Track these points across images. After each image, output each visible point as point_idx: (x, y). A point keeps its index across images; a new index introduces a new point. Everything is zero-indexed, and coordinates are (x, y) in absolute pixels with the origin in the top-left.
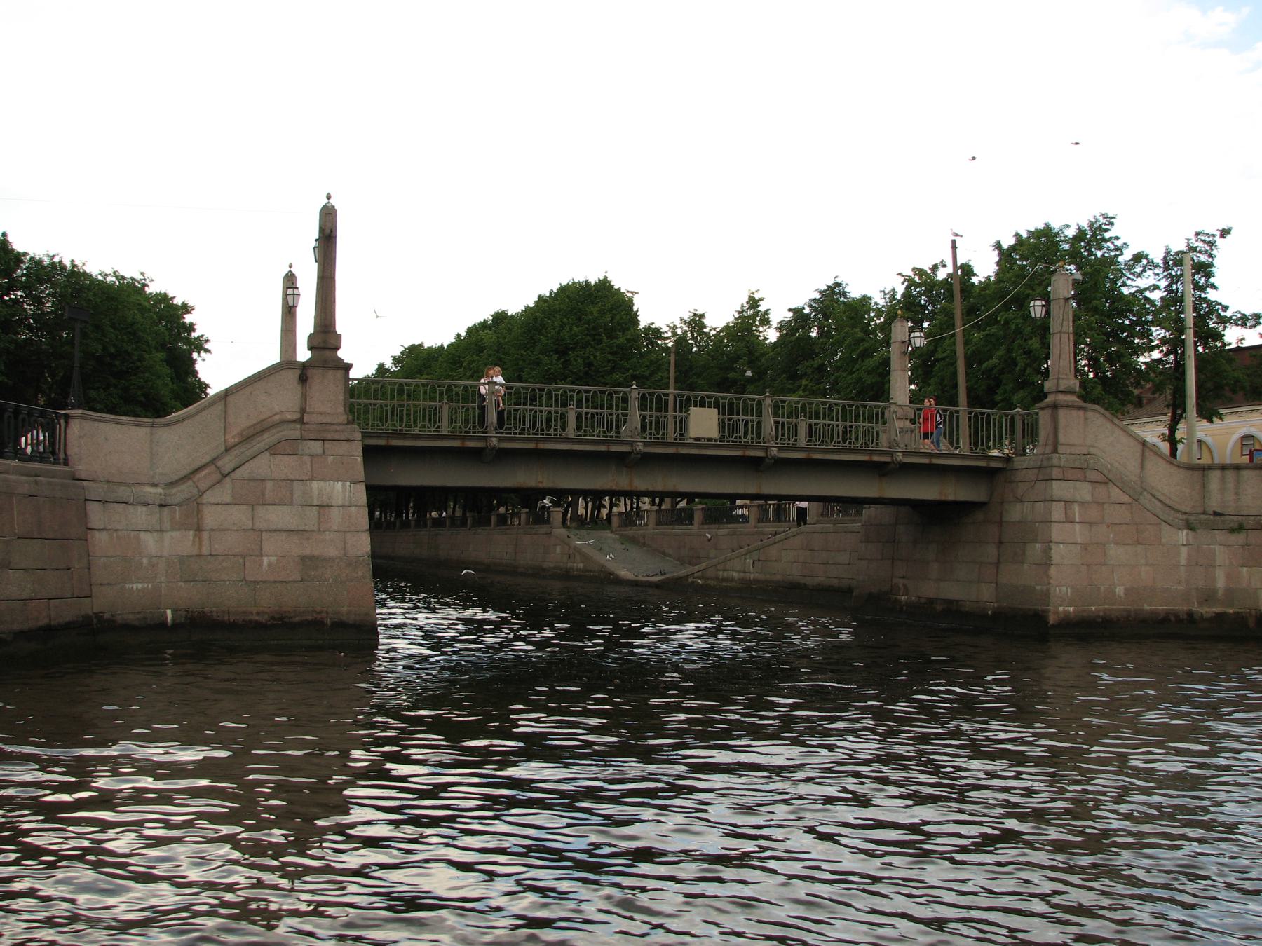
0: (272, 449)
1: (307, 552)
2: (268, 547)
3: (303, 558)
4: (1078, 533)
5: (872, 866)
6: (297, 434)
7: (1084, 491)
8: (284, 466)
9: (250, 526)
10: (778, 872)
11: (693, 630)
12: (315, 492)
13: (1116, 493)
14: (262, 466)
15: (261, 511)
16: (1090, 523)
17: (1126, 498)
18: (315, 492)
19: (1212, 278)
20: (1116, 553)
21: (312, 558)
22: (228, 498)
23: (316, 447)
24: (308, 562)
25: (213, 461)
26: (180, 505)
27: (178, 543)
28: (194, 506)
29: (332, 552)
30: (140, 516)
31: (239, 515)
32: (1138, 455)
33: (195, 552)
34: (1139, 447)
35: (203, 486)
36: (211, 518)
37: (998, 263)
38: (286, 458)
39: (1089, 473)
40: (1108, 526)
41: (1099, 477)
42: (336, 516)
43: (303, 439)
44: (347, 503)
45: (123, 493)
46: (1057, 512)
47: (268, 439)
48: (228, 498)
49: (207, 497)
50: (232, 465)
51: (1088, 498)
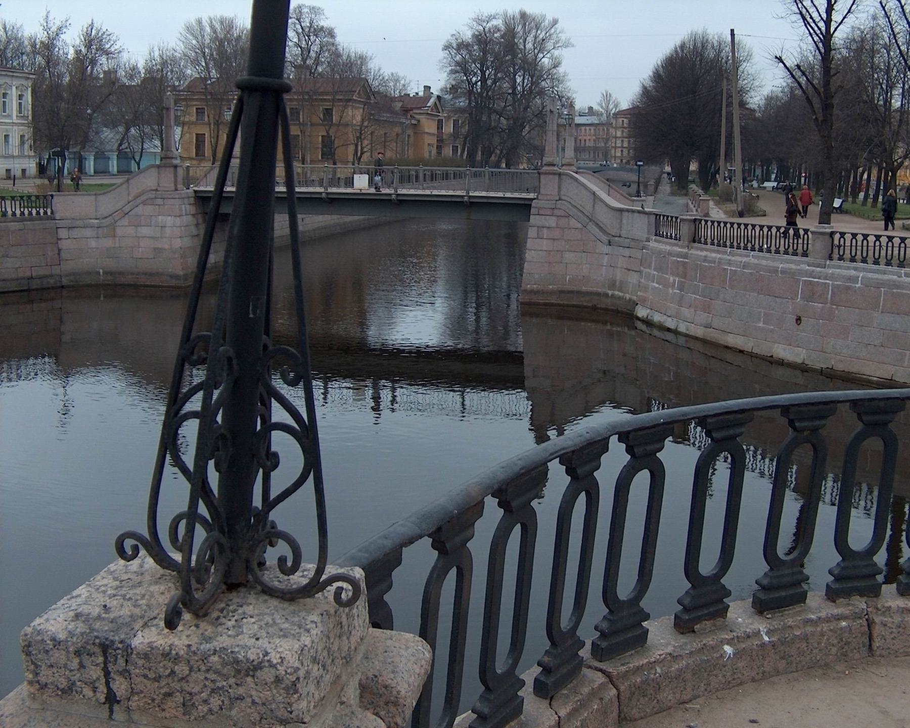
0: (144, 203)
2: (142, 244)
3: (155, 249)
4: (545, 245)
5: (425, 392)
6: (153, 196)
7: (552, 222)
8: (148, 209)
9: (135, 235)
10: (273, 474)
11: (728, 90)
12: (160, 220)
13: (573, 223)
14: (140, 210)
15: (139, 228)
16: (554, 239)
17: (579, 226)
18: (160, 220)
19: (139, 66)
20: (569, 256)
21: (157, 248)
22: (127, 224)
23: (160, 201)
24: (158, 251)
25: (121, 209)
26: (106, 227)
27: (108, 243)
28: (113, 227)
29: (166, 246)
30: (88, 232)
31: (131, 231)
32: (592, 201)
33: (113, 246)
34: (592, 196)
35: (116, 218)
36: (119, 232)
37: (645, 91)
38: (150, 206)
39: (555, 211)
41: (563, 213)
42: (168, 231)
43: (156, 198)
45: (80, 223)
46: (532, 232)
47: (143, 198)
48: (127, 224)
49: (118, 223)
50: (129, 210)
51: (554, 225)
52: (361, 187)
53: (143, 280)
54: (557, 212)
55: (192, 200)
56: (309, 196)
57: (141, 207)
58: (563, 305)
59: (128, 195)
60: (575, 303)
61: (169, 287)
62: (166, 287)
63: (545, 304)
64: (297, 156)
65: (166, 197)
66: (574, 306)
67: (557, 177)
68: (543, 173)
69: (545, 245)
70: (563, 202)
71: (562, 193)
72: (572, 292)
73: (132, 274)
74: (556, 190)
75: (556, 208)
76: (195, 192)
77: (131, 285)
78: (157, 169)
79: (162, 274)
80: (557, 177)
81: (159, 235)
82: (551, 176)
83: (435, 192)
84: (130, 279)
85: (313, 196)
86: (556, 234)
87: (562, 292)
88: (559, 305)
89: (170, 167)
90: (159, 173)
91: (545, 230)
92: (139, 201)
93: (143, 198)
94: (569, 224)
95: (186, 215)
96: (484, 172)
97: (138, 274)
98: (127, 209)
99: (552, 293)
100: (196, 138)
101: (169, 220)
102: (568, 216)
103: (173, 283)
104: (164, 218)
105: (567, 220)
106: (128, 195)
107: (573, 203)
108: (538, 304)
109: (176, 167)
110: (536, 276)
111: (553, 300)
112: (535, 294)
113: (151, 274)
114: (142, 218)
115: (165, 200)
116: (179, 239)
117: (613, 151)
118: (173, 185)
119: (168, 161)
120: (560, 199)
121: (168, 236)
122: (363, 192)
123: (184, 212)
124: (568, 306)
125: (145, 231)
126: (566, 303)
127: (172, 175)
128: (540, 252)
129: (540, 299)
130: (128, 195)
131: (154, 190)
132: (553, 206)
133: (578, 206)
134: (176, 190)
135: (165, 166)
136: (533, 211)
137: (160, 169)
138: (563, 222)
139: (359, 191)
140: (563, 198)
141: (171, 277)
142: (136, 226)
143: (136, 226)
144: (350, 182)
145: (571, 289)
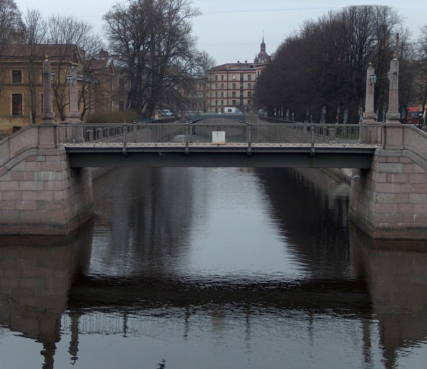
1: (39, 199)
3: (37, 201)
4: (394, 188)
6: (35, 153)
7: (399, 168)
8: (30, 166)
13: (417, 168)
14: (22, 166)
15: (22, 183)
16: (401, 183)
20: (414, 197)
21: (41, 201)
22: (9, 179)
23: (42, 158)
24: (40, 203)
29: (49, 199)
31: (14, 185)
40: (411, 184)
41: (408, 161)
42: (50, 185)
44: (55, 180)
47: (25, 155)
48: (9, 179)
51: (400, 171)
52: (219, 142)
53: (26, 230)
54: (403, 160)
55: (65, 157)
56: (173, 151)
57: (23, 163)
58: (412, 240)
59: (9, 153)
60: (422, 238)
61: (52, 235)
62: (49, 235)
63: (396, 239)
64: (20, 112)
65: (47, 154)
66: (421, 240)
67: (52, 129)
68: (389, 127)
69: (394, 188)
70: (407, 151)
71: (405, 143)
72: (419, 228)
73: (16, 224)
74: (401, 141)
75: (402, 157)
76: (67, 149)
77: (15, 235)
78: (37, 129)
79: (45, 224)
80: (401, 130)
81: (41, 188)
82: (396, 129)
83: (284, 145)
84: (13, 230)
85: (176, 151)
86: (403, 178)
87: (409, 228)
88: (408, 240)
89: (50, 127)
90: (39, 133)
91: (393, 175)
92: (20, 158)
93: (25, 155)
94: (413, 170)
95: (64, 170)
96: (132, 127)
97: (22, 224)
98: (9, 165)
99: (401, 229)
100: (13, 98)
101: (51, 175)
102: (413, 163)
103: (57, 231)
104: (47, 173)
105: (411, 166)
106: (9, 153)
107: (416, 151)
108: (391, 239)
109: (55, 127)
110: (387, 215)
111: (403, 235)
112: (387, 231)
113: (35, 225)
114: (25, 173)
115: (47, 157)
116: (61, 192)
117: (209, 101)
118: (53, 143)
119: (48, 121)
120: (404, 149)
121: (50, 189)
122: (220, 146)
123: (63, 169)
124: (416, 240)
125: (26, 185)
126: (414, 237)
127: (53, 134)
128: (390, 195)
129: (390, 235)
130: (9, 153)
131: (34, 148)
132: (399, 155)
133: (420, 154)
134: (56, 147)
135: (46, 126)
136: (376, 158)
137: (41, 129)
138: (409, 168)
139: (216, 146)
140: (407, 147)
141: (55, 226)
142: (19, 181)
143: (19, 181)
144: (209, 138)
145: (419, 226)
